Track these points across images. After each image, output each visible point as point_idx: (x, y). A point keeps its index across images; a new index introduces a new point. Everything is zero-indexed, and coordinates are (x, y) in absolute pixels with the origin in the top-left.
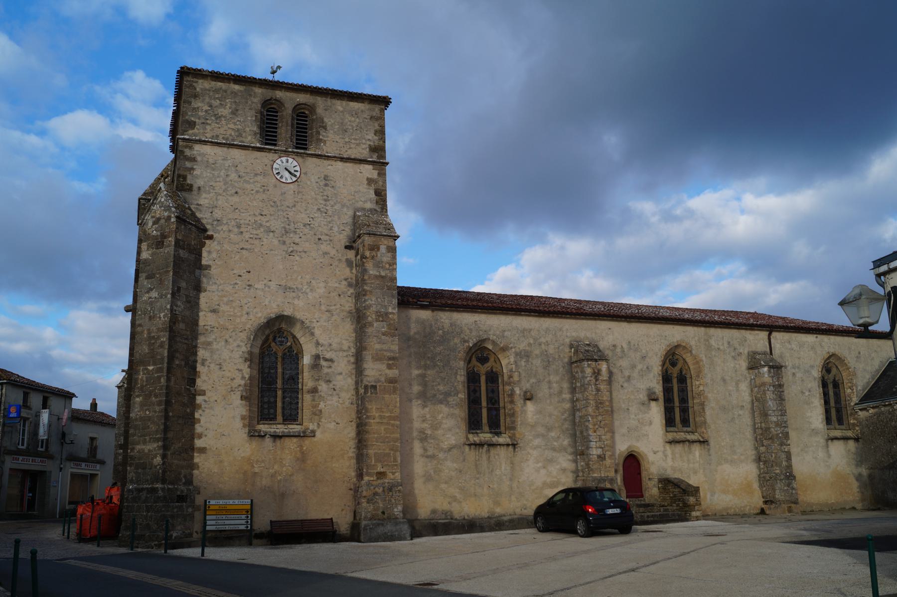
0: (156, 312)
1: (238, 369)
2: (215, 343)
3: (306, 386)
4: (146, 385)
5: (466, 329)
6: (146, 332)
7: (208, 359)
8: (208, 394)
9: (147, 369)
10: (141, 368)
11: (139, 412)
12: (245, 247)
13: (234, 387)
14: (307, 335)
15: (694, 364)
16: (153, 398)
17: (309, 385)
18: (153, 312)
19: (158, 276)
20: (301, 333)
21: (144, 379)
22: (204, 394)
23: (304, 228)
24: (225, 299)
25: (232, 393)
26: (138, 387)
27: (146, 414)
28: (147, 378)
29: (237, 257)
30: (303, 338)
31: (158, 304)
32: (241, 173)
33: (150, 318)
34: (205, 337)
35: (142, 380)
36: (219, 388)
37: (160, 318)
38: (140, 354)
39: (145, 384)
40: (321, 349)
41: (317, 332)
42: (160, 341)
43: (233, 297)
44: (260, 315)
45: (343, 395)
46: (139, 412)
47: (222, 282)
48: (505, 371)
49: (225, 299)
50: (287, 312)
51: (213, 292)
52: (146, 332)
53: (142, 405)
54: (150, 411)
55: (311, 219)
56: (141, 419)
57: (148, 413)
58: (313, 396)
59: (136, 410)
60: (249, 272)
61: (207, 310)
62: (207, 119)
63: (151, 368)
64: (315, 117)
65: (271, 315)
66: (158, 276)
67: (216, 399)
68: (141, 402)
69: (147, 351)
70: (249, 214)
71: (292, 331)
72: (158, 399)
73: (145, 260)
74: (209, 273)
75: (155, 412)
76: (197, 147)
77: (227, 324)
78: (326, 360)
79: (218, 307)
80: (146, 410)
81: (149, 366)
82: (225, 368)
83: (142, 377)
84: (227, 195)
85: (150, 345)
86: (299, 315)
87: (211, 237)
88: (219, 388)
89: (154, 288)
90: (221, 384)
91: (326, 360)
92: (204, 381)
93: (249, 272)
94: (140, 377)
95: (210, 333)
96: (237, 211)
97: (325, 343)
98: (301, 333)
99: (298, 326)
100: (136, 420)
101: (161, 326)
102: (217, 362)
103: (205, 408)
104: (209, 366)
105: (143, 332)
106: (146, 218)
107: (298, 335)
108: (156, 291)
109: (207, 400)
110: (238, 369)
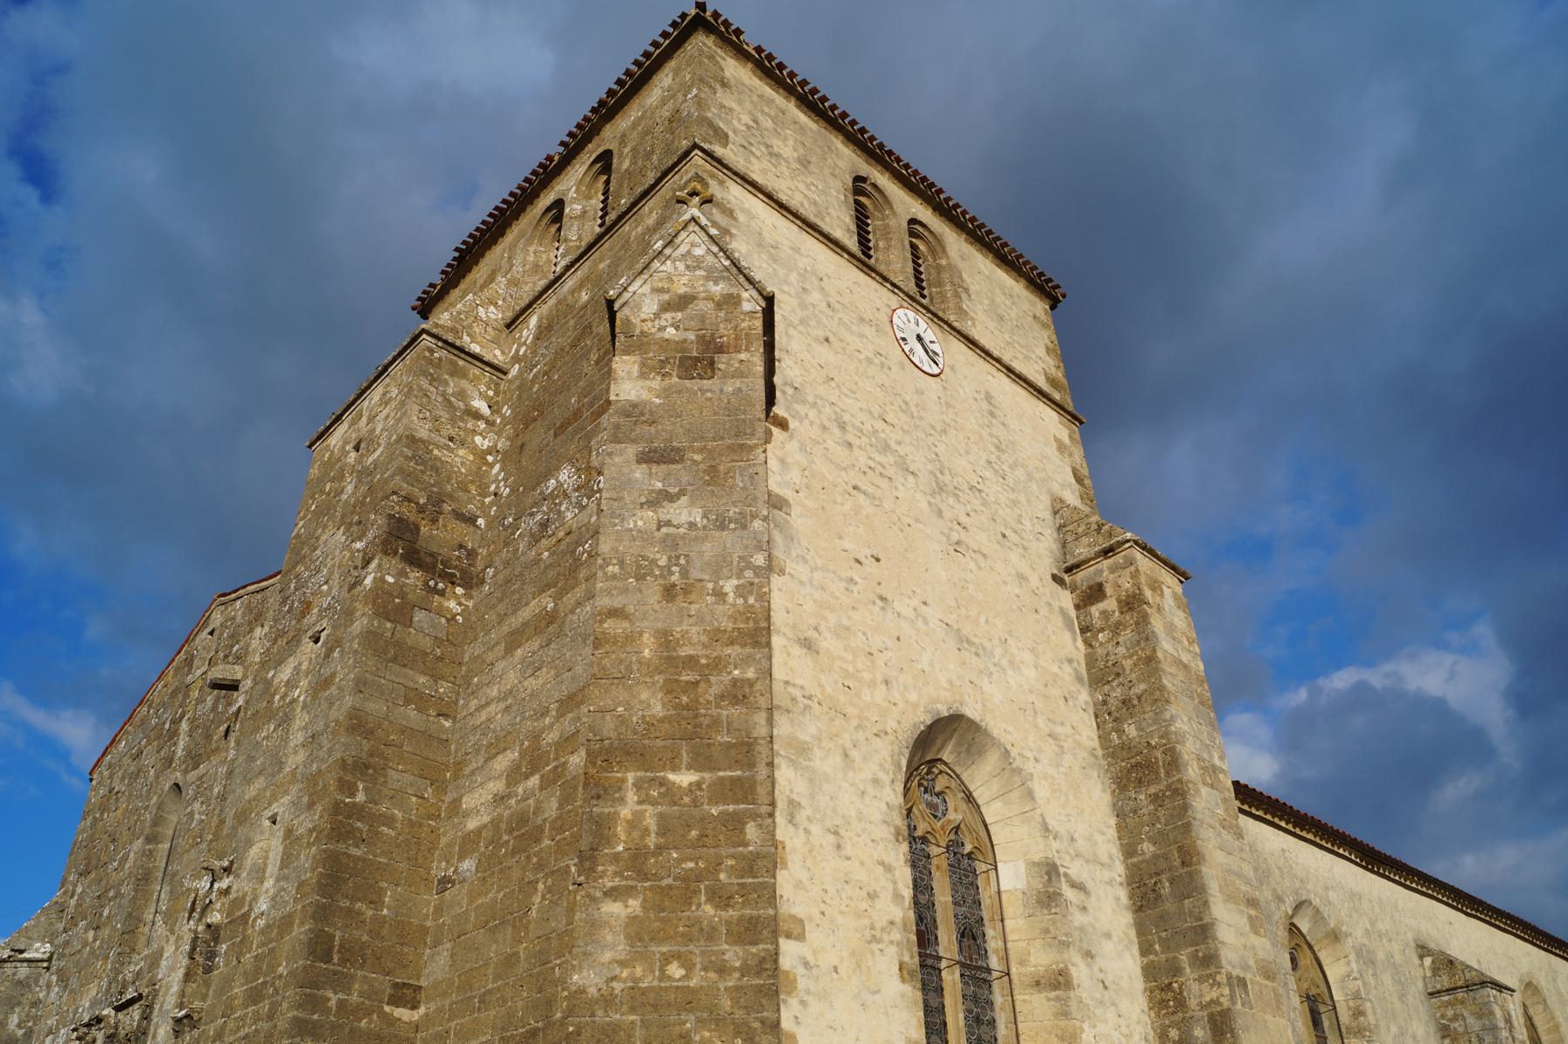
0: (695, 574)
1: (882, 863)
2: (818, 753)
3: (1022, 963)
4: (660, 849)
5: (1274, 866)
6: (648, 639)
7: (804, 803)
8: (812, 934)
9: (663, 783)
10: (631, 777)
11: (623, 964)
12: (863, 487)
13: (879, 925)
14: (1015, 795)
15: (1549, 1031)
16: (708, 909)
17: (1033, 960)
18: (685, 573)
19: (697, 457)
20: (995, 786)
21: (651, 822)
22: (801, 937)
23: (970, 492)
24: (832, 618)
25: (875, 947)
26: (616, 857)
27: (663, 976)
28: (661, 817)
29: (847, 506)
30: (997, 805)
31: (707, 546)
32: (831, 300)
33: (669, 592)
34: (792, 722)
35: (634, 823)
36: (840, 920)
37: (720, 595)
38: (622, 721)
39: (652, 841)
40: (1055, 845)
41: (1041, 790)
42: (726, 678)
43: (850, 618)
44: (913, 697)
45: (1125, 1006)
46: (623, 964)
47: (820, 563)
48: (1337, 996)
49: (832, 618)
50: (970, 712)
51: (801, 583)
52: (648, 639)
53: (638, 933)
54: (689, 967)
55: (980, 480)
56: (638, 998)
57: (675, 970)
58: (1058, 999)
59: (608, 956)
60: (878, 560)
61: (790, 634)
62: (751, 144)
63: (684, 779)
64: (944, 262)
65: (939, 706)
66: (697, 457)
67: (835, 962)
68: (633, 919)
69: (658, 709)
70: (859, 405)
71: (964, 777)
72: (732, 913)
73: (635, 405)
74: (786, 521)
75: (723, 970)
76: (735, 193)
77: (841, 698)
78: (1074, 885)
79: (816, 635)
80: (667, 959)
81: (675, 769)
82: (848, 850)
83: (638, 817)
84: (809, 335)
85: (670, 688)
86: (997, 726)
87: (783, 424)
88: (840, 920)
89: (682, 492)
90: (843, 908)
91: (1074, 885)
92: (799, 885)
93: (878, 560)
94: (625, 812)
95: (803, 713)
96: (833, 384)
97: (1061, 830)
98: (995, 786)
99: (991, 761)
100: (608, 1001)
101: (727, 625)
102: (828, 823)
103: (808, 992)
104: (806, 831)
105: (631, 639)
106: (631, 289)
107: (980, 795)
108: (692, 504)
109: (810, 958)
110: (882, 863)
